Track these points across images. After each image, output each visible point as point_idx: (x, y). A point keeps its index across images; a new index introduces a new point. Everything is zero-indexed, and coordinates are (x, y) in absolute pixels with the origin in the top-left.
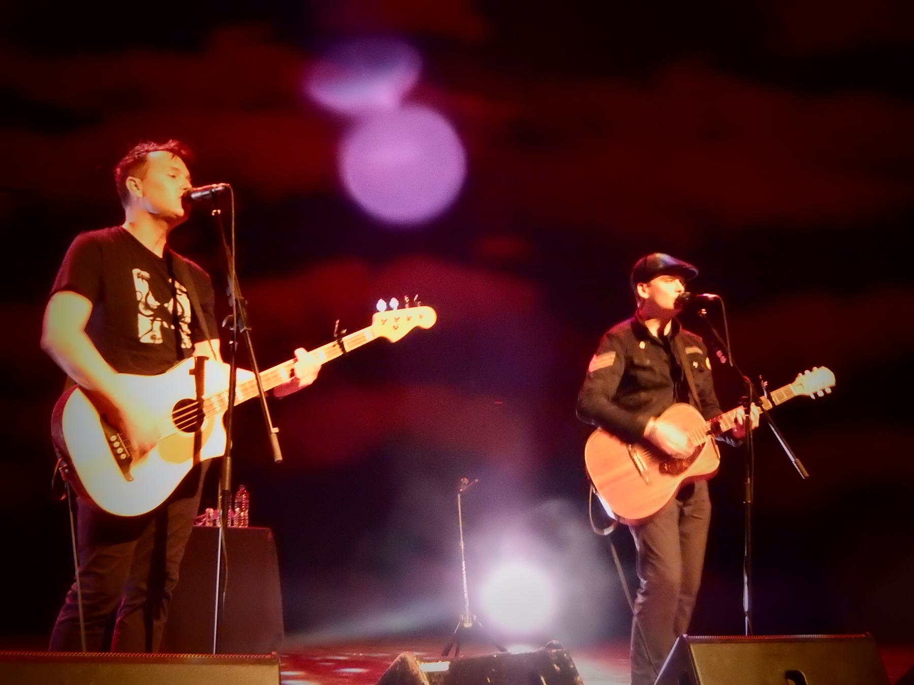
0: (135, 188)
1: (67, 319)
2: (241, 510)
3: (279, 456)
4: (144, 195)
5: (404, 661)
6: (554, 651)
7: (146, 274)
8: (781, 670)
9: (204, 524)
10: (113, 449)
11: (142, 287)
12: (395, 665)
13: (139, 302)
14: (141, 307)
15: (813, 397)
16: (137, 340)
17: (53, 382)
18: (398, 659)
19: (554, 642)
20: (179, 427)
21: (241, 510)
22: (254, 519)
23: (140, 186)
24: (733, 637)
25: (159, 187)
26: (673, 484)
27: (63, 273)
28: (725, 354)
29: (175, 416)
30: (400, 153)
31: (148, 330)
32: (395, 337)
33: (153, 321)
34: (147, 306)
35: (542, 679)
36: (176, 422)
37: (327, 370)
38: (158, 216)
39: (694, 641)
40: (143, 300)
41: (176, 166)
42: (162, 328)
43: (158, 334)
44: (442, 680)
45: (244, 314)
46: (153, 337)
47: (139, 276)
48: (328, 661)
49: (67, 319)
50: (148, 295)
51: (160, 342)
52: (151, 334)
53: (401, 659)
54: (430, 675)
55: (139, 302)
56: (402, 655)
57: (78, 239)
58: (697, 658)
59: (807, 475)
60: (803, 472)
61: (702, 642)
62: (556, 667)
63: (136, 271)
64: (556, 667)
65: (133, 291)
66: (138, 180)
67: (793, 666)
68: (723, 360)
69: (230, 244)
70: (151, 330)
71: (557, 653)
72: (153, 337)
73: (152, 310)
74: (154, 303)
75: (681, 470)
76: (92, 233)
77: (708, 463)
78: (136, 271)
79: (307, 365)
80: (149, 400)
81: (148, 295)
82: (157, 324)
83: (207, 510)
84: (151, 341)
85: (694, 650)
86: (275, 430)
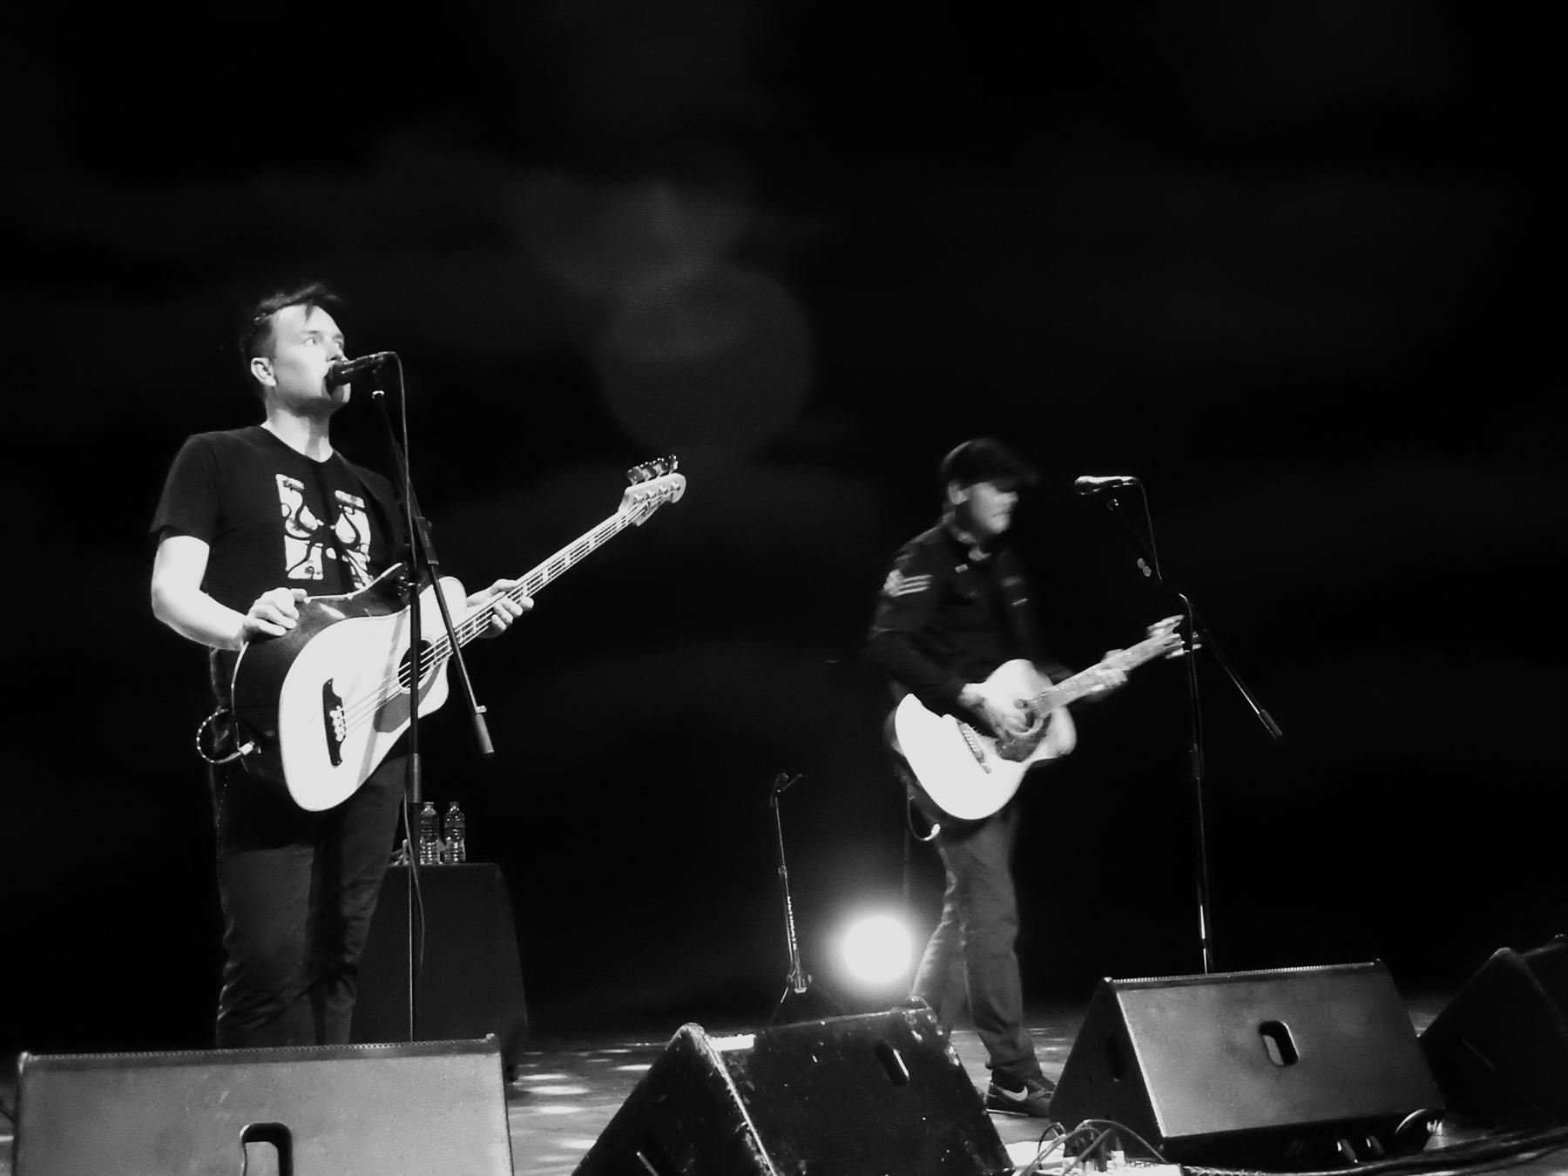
0: (264, 374)
3: (490, 749)
5: (686, 1037)
6: (912, 1012)
7: (300, 485)
8: (1253, 1020)
10: (1503, 1168)
11: (290, 496)
12: (674, 1046)
14: (289, 526)
21: (454, 839)
22: (473, 852)
23: (271, 370)
24: (1177, 978)
25: (294, 365)
27: (161, 518)
28: (1149, 563)
30: (667, 270)
33: (310, 547)
34: (299, 525)
35: (896, 1053)
38: (303, 407)
39: (1122, 987)
40: (293, 516)
42: (324, 556)
43: (318, 567)
44: (744, 1062)
46: (310, 570)
48: (602, 1056)
49: (179, 574)
51: (320, 577)
52: (306, 565)
54: (726, 1056)
56: (684, 1028)
57: (191, 441)
61: (1132, 987)
62: (918, 1037)
63: (280, 478)
64: (918, 1037)
65: (278, 505)
66: (264, 360)
67: (1270, 1013)
68: (1147, 572)
69: (400, 439)
71: (916, 1015)
72: (310, 570)
76: (203, 435)
77: (1063, 736)
78: (280, 478)
82: (316, 551)
84: (307, 576)
86: (481, 709)
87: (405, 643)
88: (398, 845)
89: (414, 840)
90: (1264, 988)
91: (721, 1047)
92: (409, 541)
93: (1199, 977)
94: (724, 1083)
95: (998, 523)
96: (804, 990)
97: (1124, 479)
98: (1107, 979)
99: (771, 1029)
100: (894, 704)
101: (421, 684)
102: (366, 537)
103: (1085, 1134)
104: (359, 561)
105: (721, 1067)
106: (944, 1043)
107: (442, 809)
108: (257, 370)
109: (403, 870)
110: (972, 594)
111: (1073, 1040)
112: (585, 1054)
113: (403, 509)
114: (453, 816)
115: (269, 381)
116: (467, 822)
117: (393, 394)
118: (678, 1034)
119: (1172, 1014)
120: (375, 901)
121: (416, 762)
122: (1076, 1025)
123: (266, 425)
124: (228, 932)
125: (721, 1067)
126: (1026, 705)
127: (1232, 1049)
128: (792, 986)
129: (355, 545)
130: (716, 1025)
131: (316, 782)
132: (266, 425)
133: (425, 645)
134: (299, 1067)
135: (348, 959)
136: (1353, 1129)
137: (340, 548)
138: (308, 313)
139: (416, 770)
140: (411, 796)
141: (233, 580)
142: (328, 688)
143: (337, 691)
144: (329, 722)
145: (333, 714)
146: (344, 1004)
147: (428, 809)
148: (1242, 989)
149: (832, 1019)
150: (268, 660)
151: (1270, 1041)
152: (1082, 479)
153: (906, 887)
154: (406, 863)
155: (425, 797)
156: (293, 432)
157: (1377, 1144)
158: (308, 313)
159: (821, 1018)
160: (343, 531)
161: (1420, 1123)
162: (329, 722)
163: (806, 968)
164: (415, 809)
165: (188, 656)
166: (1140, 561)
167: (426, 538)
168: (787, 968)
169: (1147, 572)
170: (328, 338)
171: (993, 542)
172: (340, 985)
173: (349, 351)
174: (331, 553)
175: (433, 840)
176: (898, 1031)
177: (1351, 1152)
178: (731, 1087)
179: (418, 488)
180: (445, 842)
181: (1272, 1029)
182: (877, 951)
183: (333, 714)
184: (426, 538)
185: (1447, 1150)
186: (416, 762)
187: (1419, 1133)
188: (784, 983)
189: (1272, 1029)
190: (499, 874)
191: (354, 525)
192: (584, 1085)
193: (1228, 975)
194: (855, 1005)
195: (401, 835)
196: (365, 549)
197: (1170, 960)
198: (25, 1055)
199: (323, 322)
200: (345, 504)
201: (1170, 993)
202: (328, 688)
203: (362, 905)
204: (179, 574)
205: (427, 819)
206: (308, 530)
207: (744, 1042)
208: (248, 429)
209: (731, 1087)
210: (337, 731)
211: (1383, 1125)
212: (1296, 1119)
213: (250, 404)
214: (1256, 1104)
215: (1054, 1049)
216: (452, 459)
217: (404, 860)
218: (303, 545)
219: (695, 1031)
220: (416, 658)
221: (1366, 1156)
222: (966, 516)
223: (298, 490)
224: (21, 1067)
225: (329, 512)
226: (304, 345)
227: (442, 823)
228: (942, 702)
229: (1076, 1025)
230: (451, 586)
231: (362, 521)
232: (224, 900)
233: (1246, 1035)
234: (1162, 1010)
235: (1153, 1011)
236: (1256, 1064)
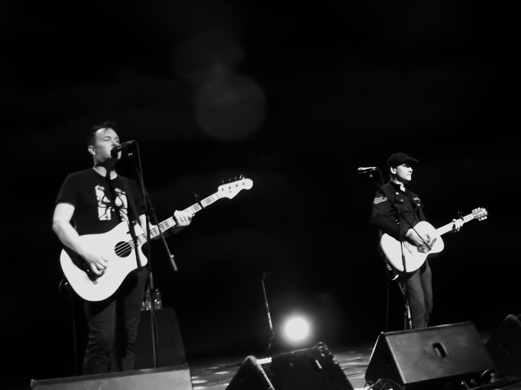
1: (63, 213)
3: (176, 268)
4: (96, 152)
5: (249, 360)
6: (321, 347)
7: (103, 188)
8: (431, 343)
10: (513, 387)
11: (100, 193)
12: (245, 363)
13: (98, 201)
14: (100, 203)
16: (98, 219)
17: (57, 245)
18: (246, 359)
20: (118, 255)
22: (164, 304)
25: (101, 147)
29: (116, 250)
31: (104, 214)
32: (231, 196)
33: (106, 210)
35: (317, 361)
36: (116, 253)
37: (196, 219)
38: (106, 164)
42: (111, 212)
45: (150, 202)
46: (106, 217)
47: (99, 189)
49: (63, 213)
51: (109, 219)
52: (105, 216)
54: (263, 365)
55: (98, 201)
56: (248, 357)
57: (69, 176)
58: (390, 342)
60: (176, 268)
64: (323, 355)
65: (96, 197)
66: (92, 147)
67: (436, 340)
69: (139, 169)
72: (106, 217)
74: (106, 200)
77: (439, 247)
79: (184, 216)
80: (96, 246)
82: (109, 211)
83: (100, 131)
84: (105, 219)
85: (387, 338)
86: (172, 256)
90: (433, 333)
91: (259, 362)
94: (263, 375)
95: (409, 178)
100: (379, 239)
103: (379, 384)
105: (262, 369)
106: (332, 357)
108: (90, 150)
110: (402, 200)
112: (203, 370)
113: (141, 192)
115: (94, 153)
118: (246, 359)
119: (405, 343)
125: (262, 369)
126: (428, 237)
127: (424, 353)
129: (122, 206)
130: (260, 356)
134: (124, 378)
136: (466, 377)
146: (130, 357)
151: (437, 350)
157: (475, 382)
161: (488, 374)
170: (113, 139)
171: (407, 184)
173: (121, 142)
174: (113, 210)
176: (316, 354)
177: (466, 385)
178: (265, 376)
179: (146, 184)
181: (437, 346)
182: (297, 329)
185: (495, 382)
187: (488, 377)
189: (437, 346)
191: (121, 200)
192: (205, 379)
194: (290, 349)
196: (126, 207)
198: (32, 380)
199: (112, 133)
207: (268, 360)
208: (87, 171)
209: (265, 376)
211: (476, 375)
212: (448, 375)
213: (88, 161)
214: (436, 370)
218: (104, 209)
219: (252, 358)
221: (471, 386)
222: (397, 177)
224: (32, 384)
226: (107, 140)
228: (401, 237)
231: (124, 198)
233: (429, 348)
234: (400, 341)
235: (398, 343)
236: (433, 357)
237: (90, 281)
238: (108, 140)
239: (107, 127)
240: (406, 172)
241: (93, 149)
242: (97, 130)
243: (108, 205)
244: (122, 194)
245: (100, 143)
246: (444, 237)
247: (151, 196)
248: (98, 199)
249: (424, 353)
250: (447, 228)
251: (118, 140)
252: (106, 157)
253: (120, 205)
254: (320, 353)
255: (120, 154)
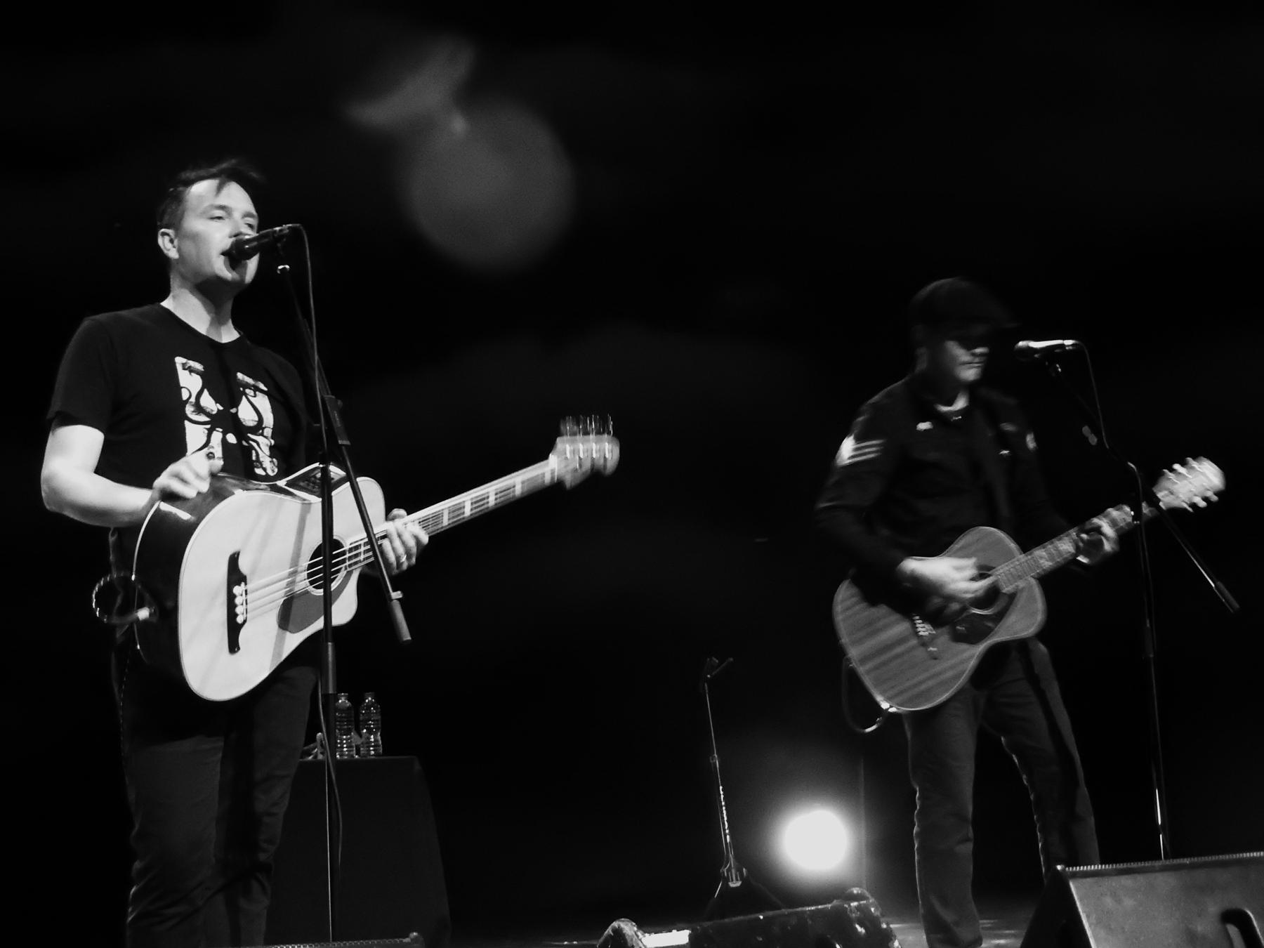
2: (370, 732)
3: (406, 635)
5: (619, 933)
6: (854, 904)
8: (1214, 909)
9: (316, 757)
14: (189, 410)
15: (1202, 504)
19: (855, 891)
21: (370, 732)
22: (389, 744)
24: (1133, 865)
25: (195, 237)
26: (972, 654)
27: (56, 405)
28: (1096, 432)
33: (210, 432)
34: (199, 409)
38: (208, 289)
39: (1075, 875)
40: (193, 400)
41: (223, 200)
42: (224, 442)
43: (218, 451)
47: (184, 367)
49: (73, 462)
50: (200, 394)
52: (206, 450)
53: (615, 930)
56: (615, 924)
57: (86, 323)
59: (1237, 606)
60: (406, 635)
62: (860, 929)
63: (179, 360)
64: (860, 929)
66: (170, 231)
68: (1093, 440)
70: (206, 445)
71: (858, 908)
73: (208, 414)
74: (208, 402)
75: (986, 633)
77: (1025, 621)
78: (179, 360)
81: (200, 394)
82: (217, 436)
83: (201, 190)
86: (396, 595)
87: (314, 537)
88: (311, 739)
89: (330, 735)
90: (1222, 876)
92: (319, 421)
93: (1157, 864)
96: (739, 884)
97: (1069, 342)
98: (1059, 867)
99: (707, 924)
101: (334, 586)
102: (269, 420)
104: (263, 445)
107: (356, 700)
108: (163, 242)
109: (318, 765)
111: (1023, 932)
114: (368, 707)
115: (173, 254)
116: (382, 714)
117: (298, 265)
118: (609, 931)
119: (1129, 903)
120: (288, 795)
121: (330, 649)
122: (1026, 915)
123: (165, 304)
124: (134, 833)
128: (727, 880)
129: (258, 428)
131: (221, 662)
132: (165, 304)
133: (338, 545)
135: (262, 857)
137: (241, 430)
138: (219, 189)
139: (330, 659)
140: (326, 686)
141: (129, 459)
142: (234, 560)
143: (244, 566)
144: (231, 598)
145: (237, 590)
147: (342, 700)
148: (1201, 876)
149: (770, 913)
150: (166, 543)
151: (1233, 930)
152: (1021, 344)
153: (862, 794)
154: (320, 757)
155: (340, 688)
156: (188, 308)
158: (219, 189)
159: (760, 912)
160: (246, 414)
162: (231, 598)
163: (742, 860)
164: (329, 700)
165: (90, 536)
166: (1086, 430)
167: (336, 416)
168: (720, 860)
169: (1093, 440)
170: (237, 215)
172: (255, 886)
174: (231, 438)
175: (348, 732)
180: (360, 735)
181: (1234, 917)
183: (237, 590)
184: (336, 416)
186: (330, 649)
188: (718, 877)
189: (1234, 917)
190: (417, 767)
191: (256, 408)
193: (1187, 861)
195: (313, 727)
196: (268, 432)
197: (1126, 847)
199: (237, 198)
200: (247, 386)
201: (1126, 881)
202: (234, 560)
203: (274, 801)
204: (73, 462)
205: (341, 711)
206: (208, 414)
208: (146, 308)
210: (239, 610)
215: (1002, 942)
216: (364, 358)
217: (318, 754)
220: (328, 555)
223: (198, 372)
225: (229, 395)
227: (357, 714)
229: (1026, 915)
230: (371, 489)
231: (263, 403)
232: (132, 796)
233: (1206, 925)
234: (1114, 895)
235: (1108, 901)
237: (276, 626)
238: (219, 218)
239: (227, 176)
240: (847, 449)
241: (172, 241)
242: (190, 183)
243: (215, 422)
244: (256, 389)
245: (194, 223)
246: (1051, 582)
247: (340, 402)
248: (185, 396)
249: (1191, 937)
250: (1044, 558)
251: (254, 221)
252: (207, 270)
253: (251, 424)
254: (850, 923)
255: (252, 265)
